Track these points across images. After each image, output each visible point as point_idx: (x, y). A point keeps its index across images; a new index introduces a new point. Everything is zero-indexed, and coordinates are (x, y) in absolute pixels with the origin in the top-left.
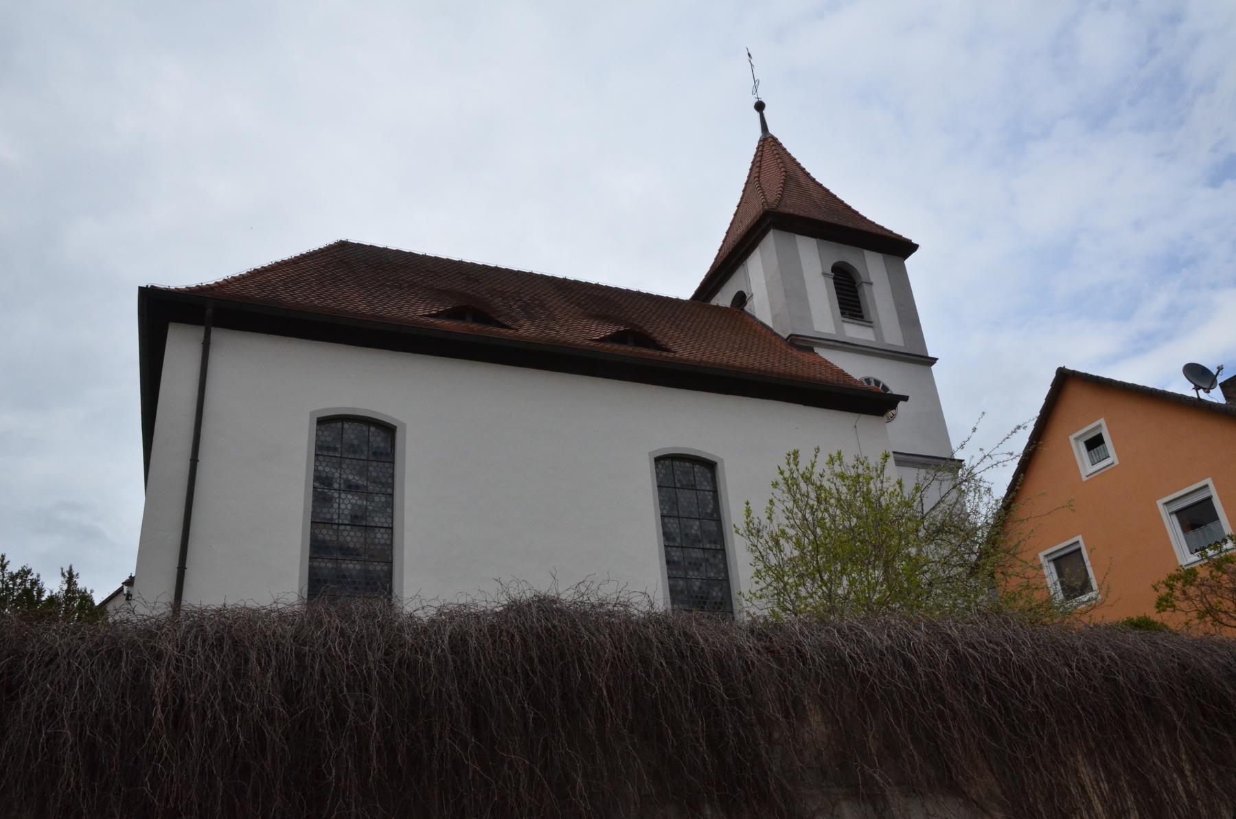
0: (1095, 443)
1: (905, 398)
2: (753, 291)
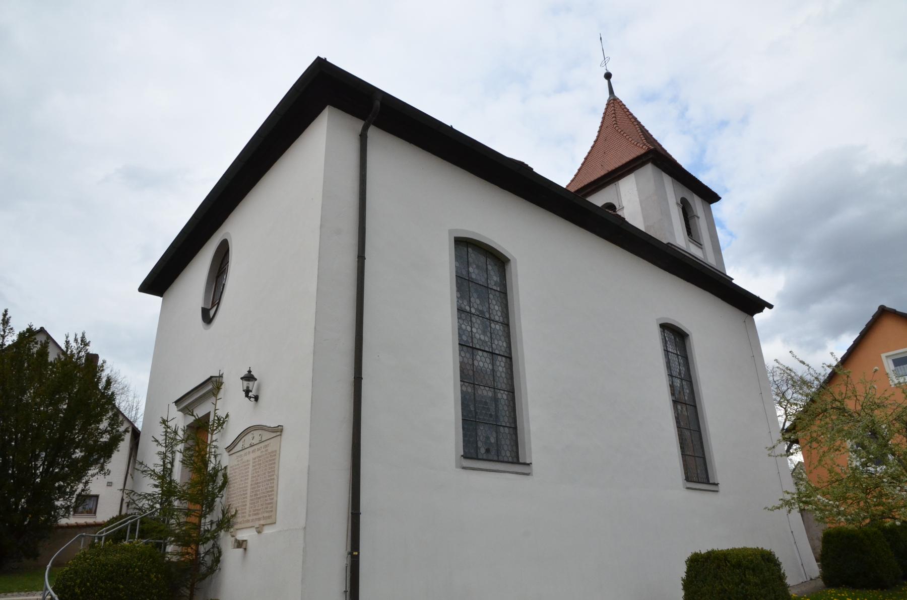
2: (624, 204)
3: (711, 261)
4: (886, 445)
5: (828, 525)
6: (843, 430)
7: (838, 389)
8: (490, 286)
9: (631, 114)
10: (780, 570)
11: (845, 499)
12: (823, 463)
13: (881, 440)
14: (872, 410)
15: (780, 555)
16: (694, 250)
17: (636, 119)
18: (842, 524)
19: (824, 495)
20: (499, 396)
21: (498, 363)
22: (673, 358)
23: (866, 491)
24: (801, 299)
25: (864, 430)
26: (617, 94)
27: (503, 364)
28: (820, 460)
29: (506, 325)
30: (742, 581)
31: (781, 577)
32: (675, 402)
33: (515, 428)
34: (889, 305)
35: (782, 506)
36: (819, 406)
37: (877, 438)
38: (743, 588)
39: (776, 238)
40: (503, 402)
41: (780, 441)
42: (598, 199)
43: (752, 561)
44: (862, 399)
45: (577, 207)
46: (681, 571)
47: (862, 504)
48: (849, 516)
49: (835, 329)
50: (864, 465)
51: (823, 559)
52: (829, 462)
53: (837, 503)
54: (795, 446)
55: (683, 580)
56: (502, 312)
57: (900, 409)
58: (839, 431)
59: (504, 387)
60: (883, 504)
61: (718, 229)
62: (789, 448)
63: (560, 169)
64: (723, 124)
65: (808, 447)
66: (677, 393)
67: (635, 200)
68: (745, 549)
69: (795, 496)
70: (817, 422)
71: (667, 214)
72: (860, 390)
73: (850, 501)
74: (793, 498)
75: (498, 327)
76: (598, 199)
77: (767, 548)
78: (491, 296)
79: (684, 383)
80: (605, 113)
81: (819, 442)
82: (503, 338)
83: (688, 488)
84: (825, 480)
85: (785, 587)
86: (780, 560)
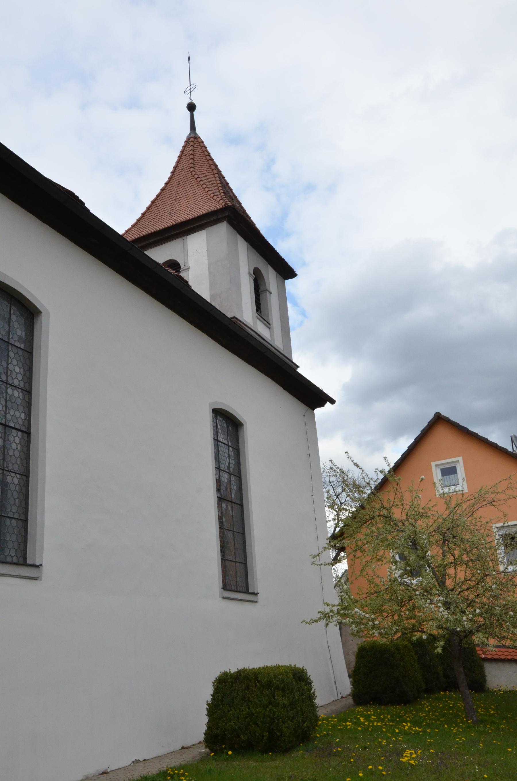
0: (449, 471)
1: (333, 402)
2: (191, 264)
3: (278, 343)
4: (424, 557)
5: (364, 639)
6: (387, 540)
7: (387, 496)
8: (11, 341)
9: (212, 160)
10: (311, 689)
11: (381, 612)
12: (365, 573)
13: (419, 552)
14: (416, 520)
15: (312, 674)
16: (261, 329)
17: (216, 166)
18: (375, 638)
19: (362, 607)
20: (9, 479)
21: (11, 439)
22: (223, 449)
23: (401, 604)
24: (366, 395)
25: (406, 540)
26: (199, 131)
27: (17, 440)
28: (362, 571)
29: (28, 391)
30: (270, 703)
31: (311, 697)
32: (220, 500)
33: (25, 521)
34: (444, 413)
35: (320, 619)
36: (368, 512)
37: (416, 549)
38: (271, 710)
39: (351, 327)
40: (13, 487)
41: (325, 549)
42: (159, 255)
43: (283, 681)
44: (407, 507)
45: (131, 260)
46: (207, 693)
47: (396, 617)
48: (382, 631)
49: (395, 431)
50: (402, 576)
51: (356, 675)
52: (370, 573)
53: (373, 616)
54: (343, 554)
55: (208, 704)
56: (24, 375)
57: (441, 520)
58: (384, 540)
59: (16, 468)
60: (414, 617)
61: (289, 306)
62: (338, 555)
63: (119, 211)
64: (310, 188)
65: (352, 556)
66: (223, 488)
67: (203, 261)
68: (278, 667)
69: (335, 609)
70: (364, 530)
71: (236, 284)
72: (407, 498)
73: (385, 614)
74: (332, 611)
75: (16, 393)
76: (159, 255)
77: (299, 665)
78: (11, 354)
79: (233, 478)
80: (182, 152)
81: (363, 551)
82: (21, 408)
83: (224, 598)
84: (365, 591)
85: (314, 707)
86: (312, 678)
